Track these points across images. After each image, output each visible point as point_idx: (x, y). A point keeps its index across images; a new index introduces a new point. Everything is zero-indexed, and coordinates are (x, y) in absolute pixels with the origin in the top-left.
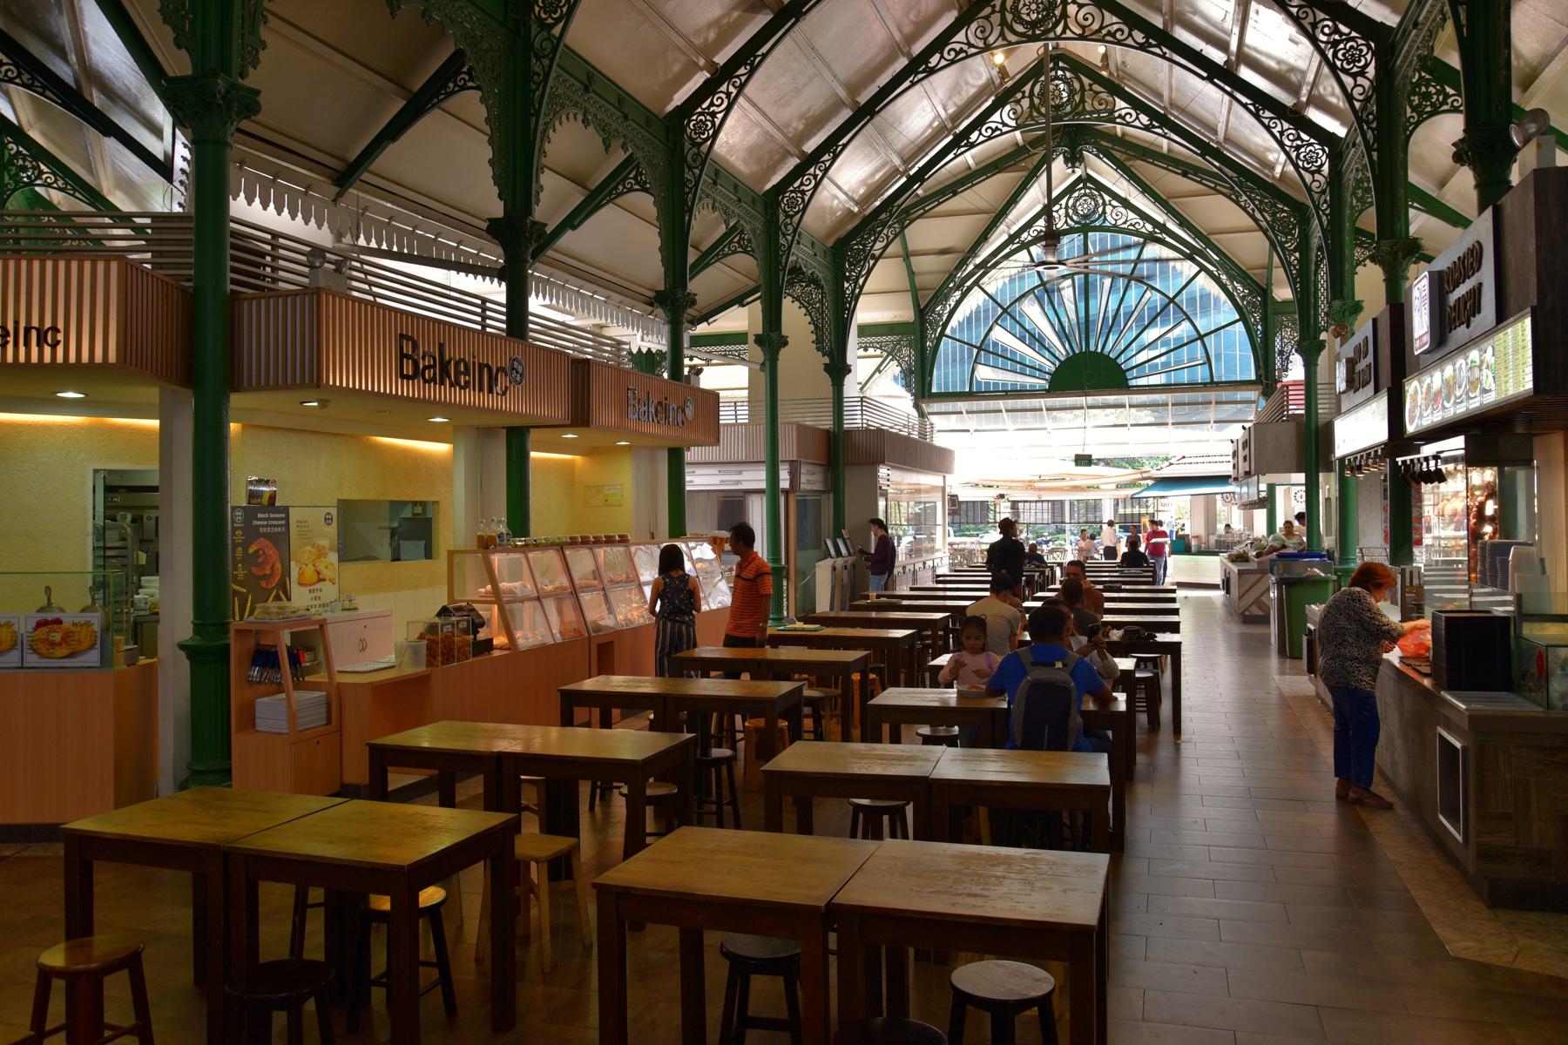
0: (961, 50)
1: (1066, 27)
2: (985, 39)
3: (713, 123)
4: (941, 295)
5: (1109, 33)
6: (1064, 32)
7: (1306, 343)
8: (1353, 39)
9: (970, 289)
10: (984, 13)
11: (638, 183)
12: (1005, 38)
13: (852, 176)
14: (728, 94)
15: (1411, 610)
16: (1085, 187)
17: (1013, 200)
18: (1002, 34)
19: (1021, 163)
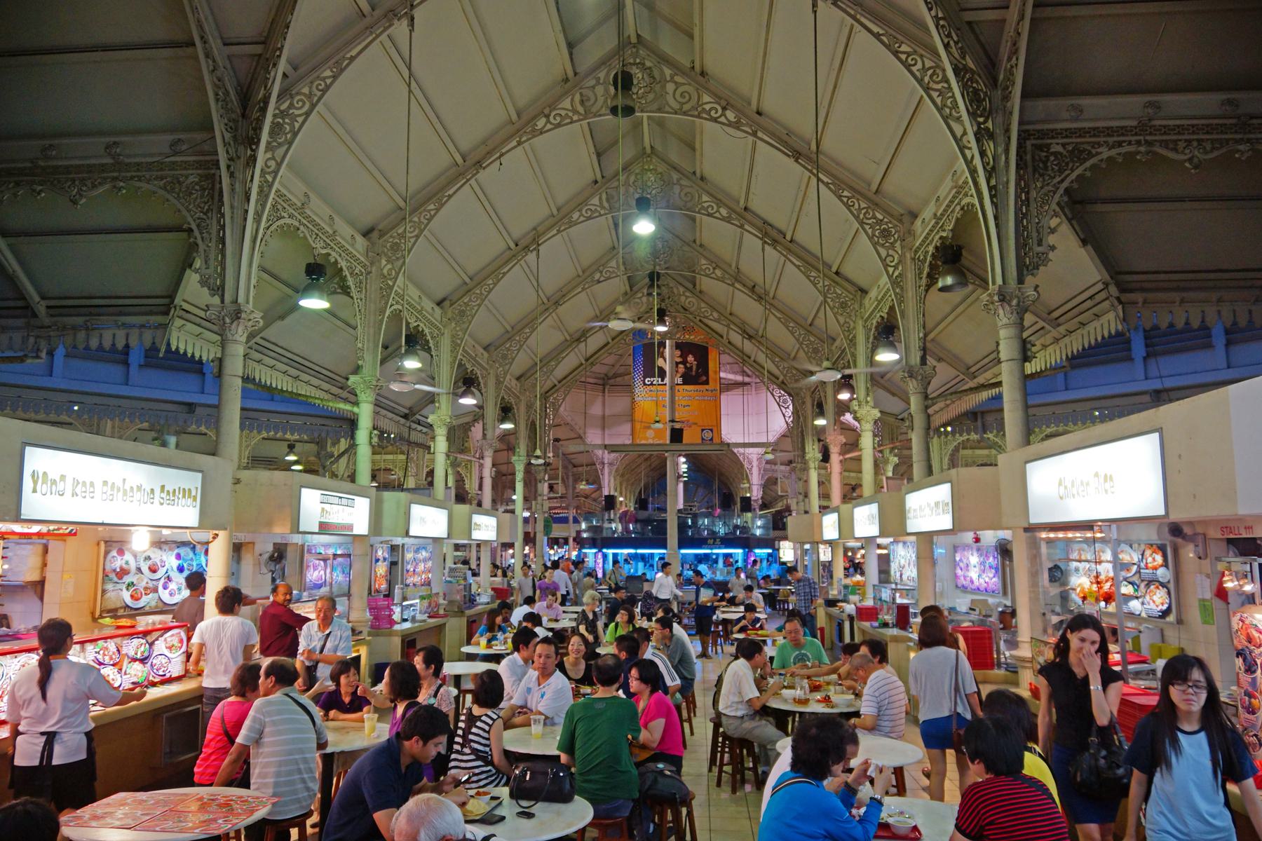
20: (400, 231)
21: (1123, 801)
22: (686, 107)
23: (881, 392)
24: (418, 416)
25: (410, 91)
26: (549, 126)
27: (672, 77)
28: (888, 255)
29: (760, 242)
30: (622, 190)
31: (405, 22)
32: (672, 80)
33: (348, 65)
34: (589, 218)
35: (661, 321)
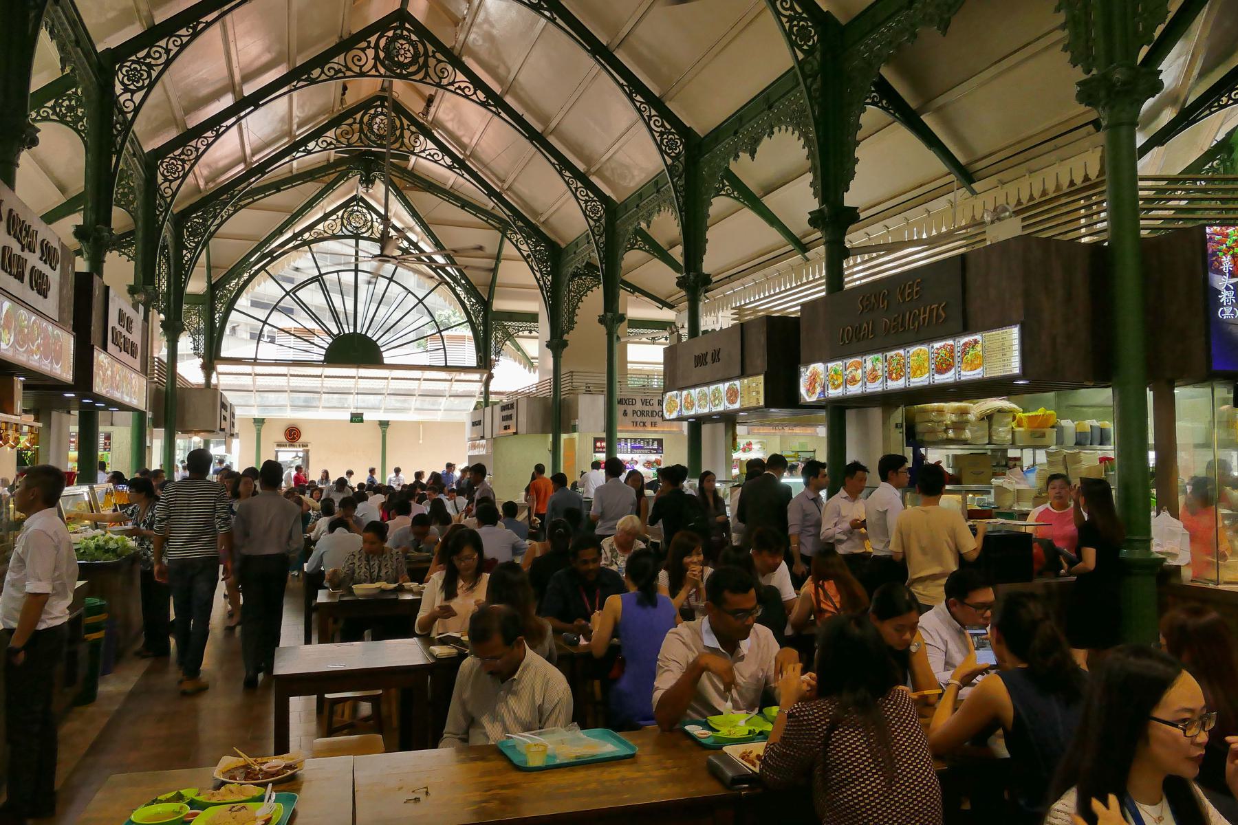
0: (340, 71)
1: (427, 74)
2: (441, 78)
3: (149, 76)
4: (235, 272)
5: (459, 88)
6: (425, 77)
7: (555, 341)
8: (672, 134)
9: (257, 272)
10: (359, 46)
11: (55, 113)
12: (377, 70)
13: (225, 150)
14: (168, 51)
15: (1224, 526)
16: (358, 205)
17: (310, 205)
18: (375, 66)
19: (326, 176)
32: (434, 56)
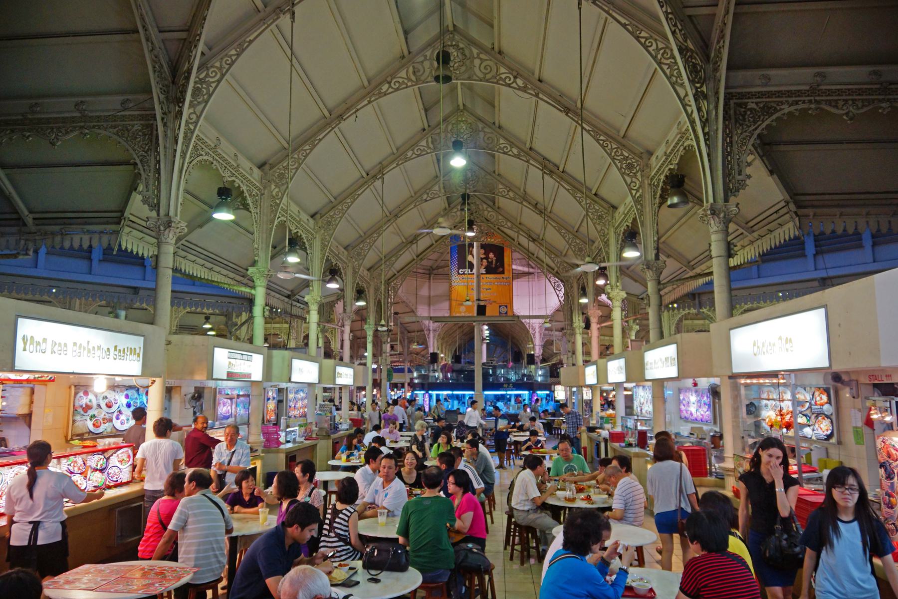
20: (285, 165)
21: (799, 570)
22: (488, 76)
23: (627, 279)
24: (297, 297)
25: (292, 65)
26: (391, 90)
27: (478, 55)
28: (632, 182)
29: (541, 173)
30: (443, 135)
31: (288, 16)
32: (478, 57)
33: (248, 46)
34: (419, 155)
35: (471, 229)
